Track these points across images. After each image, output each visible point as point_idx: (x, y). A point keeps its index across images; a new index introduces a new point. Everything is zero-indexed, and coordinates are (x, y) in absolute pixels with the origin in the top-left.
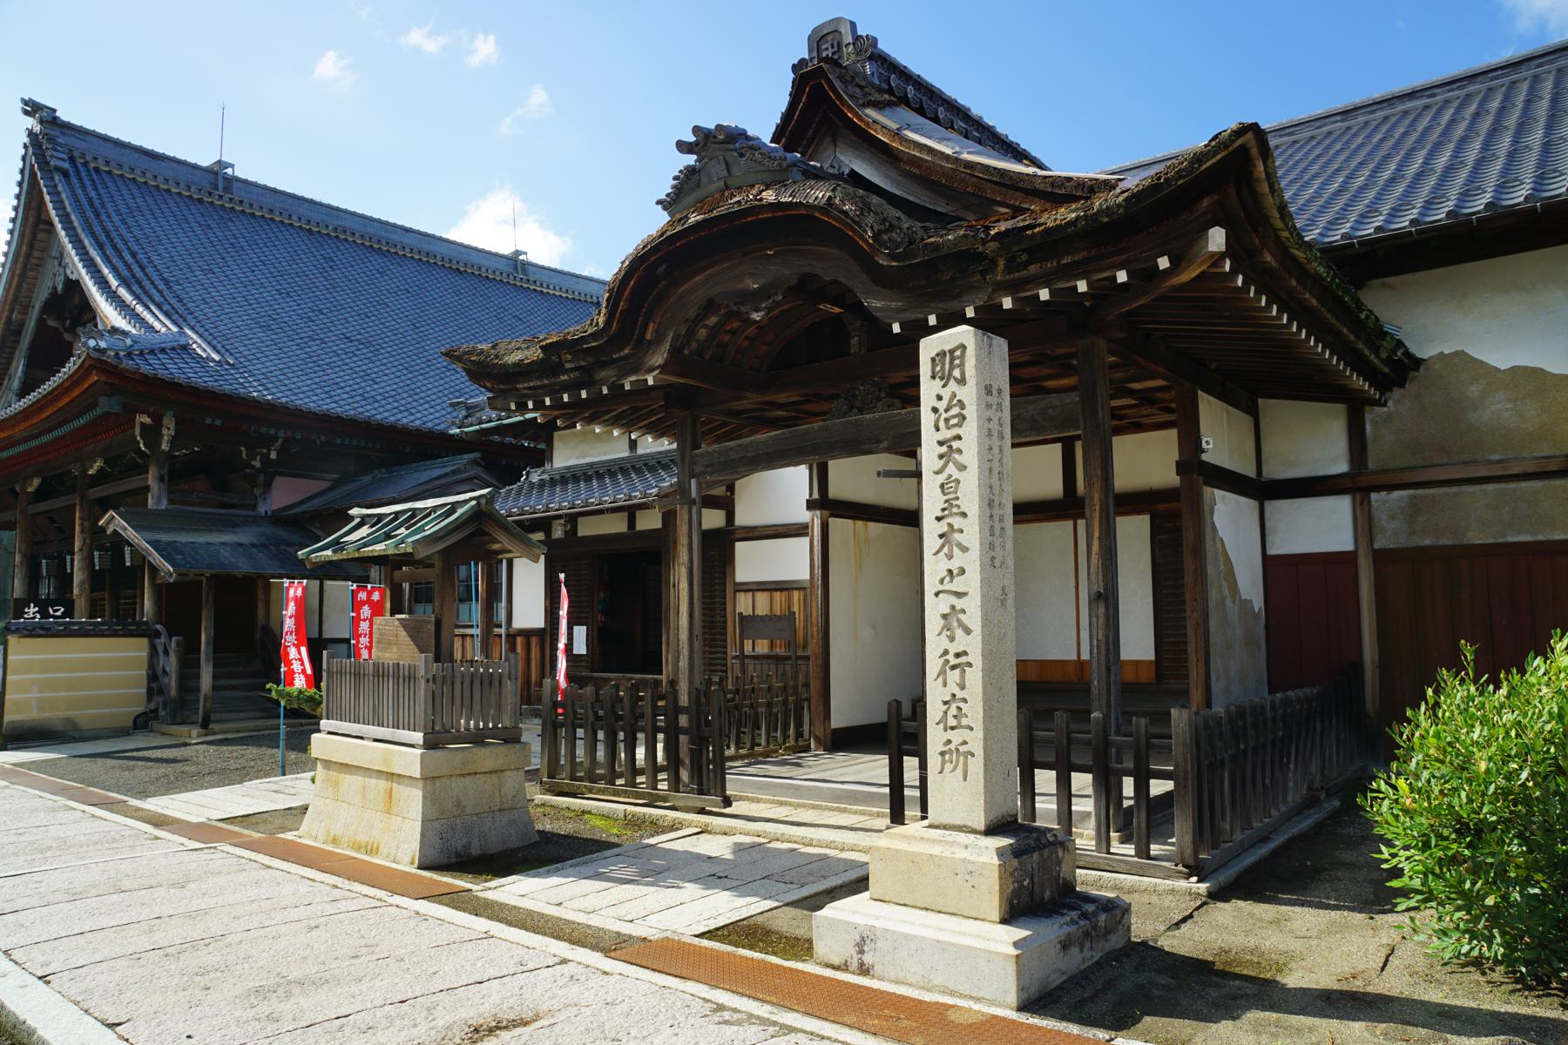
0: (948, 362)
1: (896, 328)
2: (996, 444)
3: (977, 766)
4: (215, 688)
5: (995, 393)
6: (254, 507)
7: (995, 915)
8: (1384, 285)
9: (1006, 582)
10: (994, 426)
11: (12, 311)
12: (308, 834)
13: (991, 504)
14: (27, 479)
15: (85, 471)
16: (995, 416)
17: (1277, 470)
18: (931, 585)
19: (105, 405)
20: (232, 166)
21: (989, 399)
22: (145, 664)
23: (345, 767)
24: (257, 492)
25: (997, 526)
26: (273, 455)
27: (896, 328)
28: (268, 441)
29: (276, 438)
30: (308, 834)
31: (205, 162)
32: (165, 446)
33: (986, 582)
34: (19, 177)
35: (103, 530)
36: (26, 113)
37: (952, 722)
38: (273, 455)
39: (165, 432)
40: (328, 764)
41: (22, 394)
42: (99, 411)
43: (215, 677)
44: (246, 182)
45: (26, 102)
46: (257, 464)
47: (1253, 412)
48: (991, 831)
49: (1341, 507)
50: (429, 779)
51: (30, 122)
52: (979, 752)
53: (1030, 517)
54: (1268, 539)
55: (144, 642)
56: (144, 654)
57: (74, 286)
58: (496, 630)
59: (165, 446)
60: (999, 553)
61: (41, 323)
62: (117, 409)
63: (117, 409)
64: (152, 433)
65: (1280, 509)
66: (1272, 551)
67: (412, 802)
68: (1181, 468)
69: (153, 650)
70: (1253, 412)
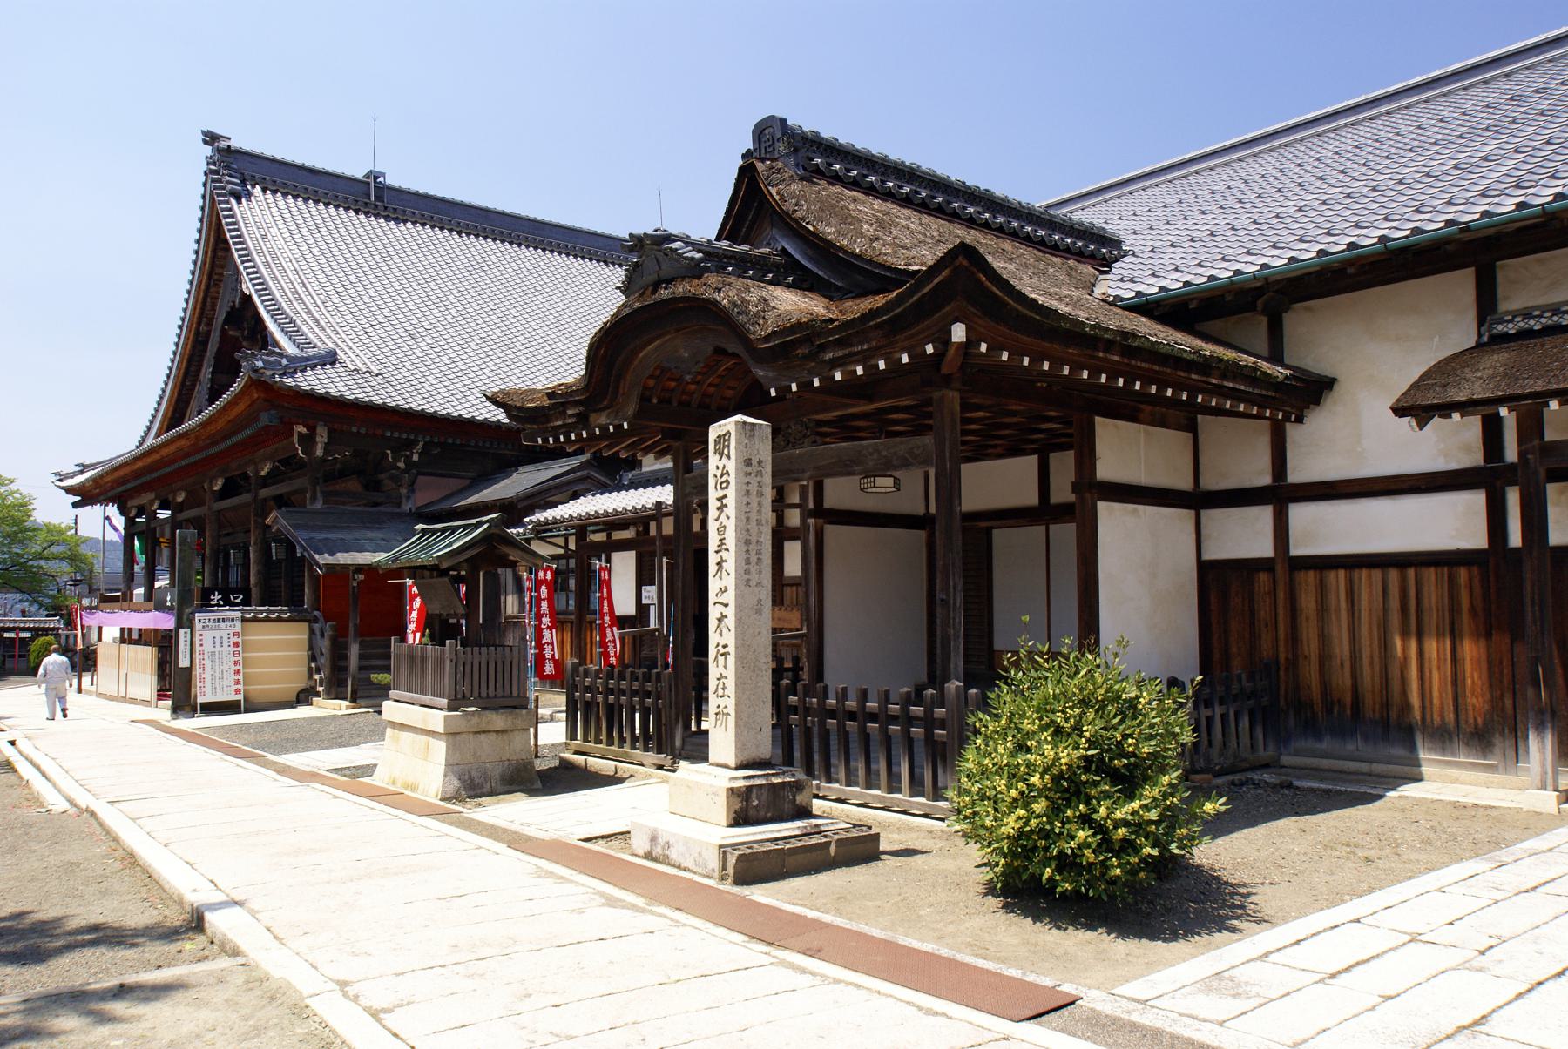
0: (723, 439)
1: (773, 393)
2: (754, 500)
3: (732, 720)
4: (361, 668)
5: (754, 463)
6: (399, 505)
7: (724, 823)
8: (1307, 309)
9: (763, 597)
10: (754, 488)
11: (199, 324)
12: (377, 780)
13: (747, 542)
14: (214, 478)
15: (257, 472)
16: (754, 481)
17: (1213, 481)
18: (712, 598)
19: (264, 419)
20: (384, 175)
21: (749, 469)
22: (306, 646)
23: (402, 727)
24: (404, 491)
25: (754, 559)
26: (415, 457)
27: (773, 393)
28: (411, 445)
29: (415, 443)
30: (377, 780)
31: (359, 174)
32: (319, 453)
33: (739, 596)
34: (201, 202)
35: (269, 527)
36: (205, 142)
37: (720, 692)
38: (415, 457)
39: (318, 439)
40: (394, 725)
41: (211, 401)
42: (261, 424)
43: (361, 657)
44: (400, 191)
45: (205, 134)
46: (401, 465)
47: (1192, 428)
48: (738, 767)
49: (1263, 516)
50: (451, 735)
51: (208, 150)
52: (733, 713)
53: (1012, 522)
54: (1203, 545)
55: (305, 626)
56: (305, 637)
57: (247, 299)
58: (589, 617)
59: (319, 453)
60: (755, 578)
61: (223, 332)
62: (275, 422)
63: (275, 422)
64: (308, 441)
65: (1212, 517)
66: (1206, 556)
67: (440, 748)
68: (1076, 487)
69: (312, 632)
70: (1192, 428)
